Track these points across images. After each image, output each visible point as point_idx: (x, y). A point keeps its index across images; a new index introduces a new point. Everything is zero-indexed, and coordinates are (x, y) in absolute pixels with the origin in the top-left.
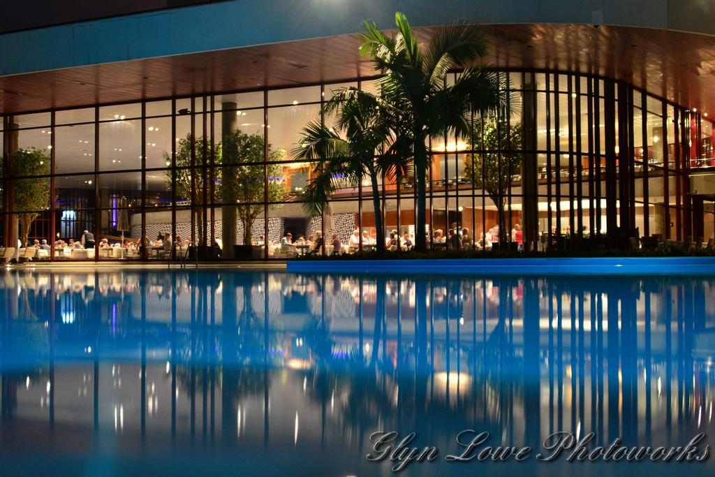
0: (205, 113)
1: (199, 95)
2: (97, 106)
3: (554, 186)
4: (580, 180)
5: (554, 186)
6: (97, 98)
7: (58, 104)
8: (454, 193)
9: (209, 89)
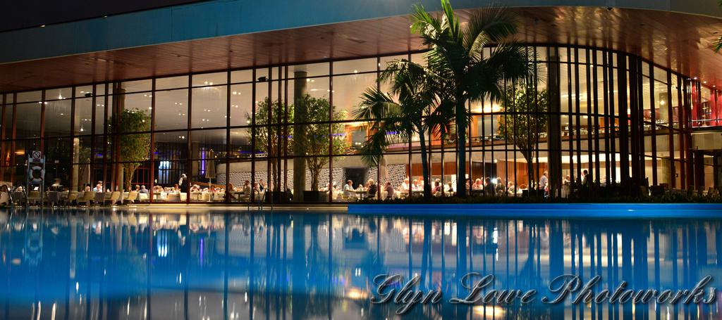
0: (280, 80)
1: (275, 66)
2: (190, 74)
3: (575, 143)
4: (597, 137)
5: (575, 143)
6: (191, 67)
7: (158, 73)
8: (490, 148)
9: (284, 61)
